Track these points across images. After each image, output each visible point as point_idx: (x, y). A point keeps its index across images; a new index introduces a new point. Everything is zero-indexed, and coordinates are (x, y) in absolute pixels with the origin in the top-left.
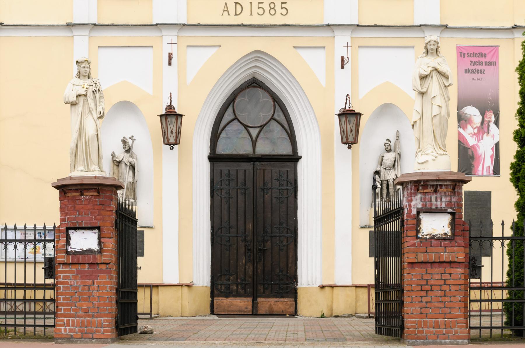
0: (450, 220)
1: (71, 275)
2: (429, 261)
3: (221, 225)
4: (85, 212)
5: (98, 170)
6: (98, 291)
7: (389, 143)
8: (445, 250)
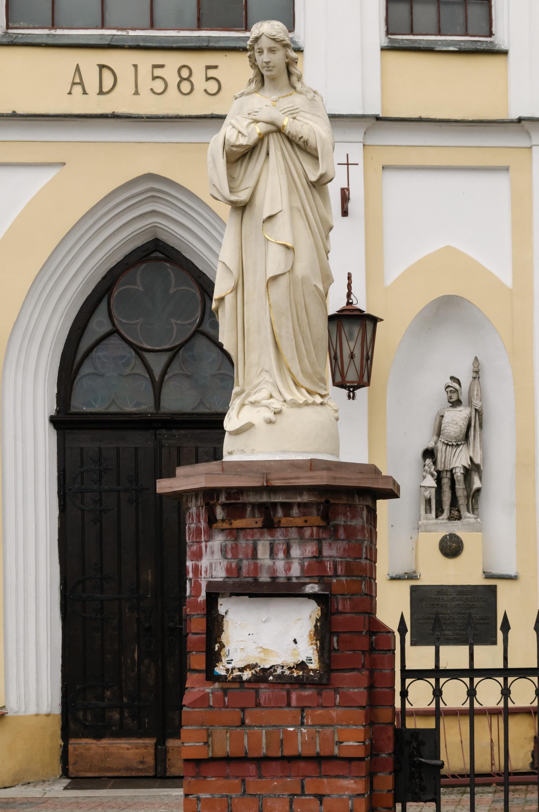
0: (317, 620)
2: (250, 755)
7: (456, 385)
8: (303, 718)
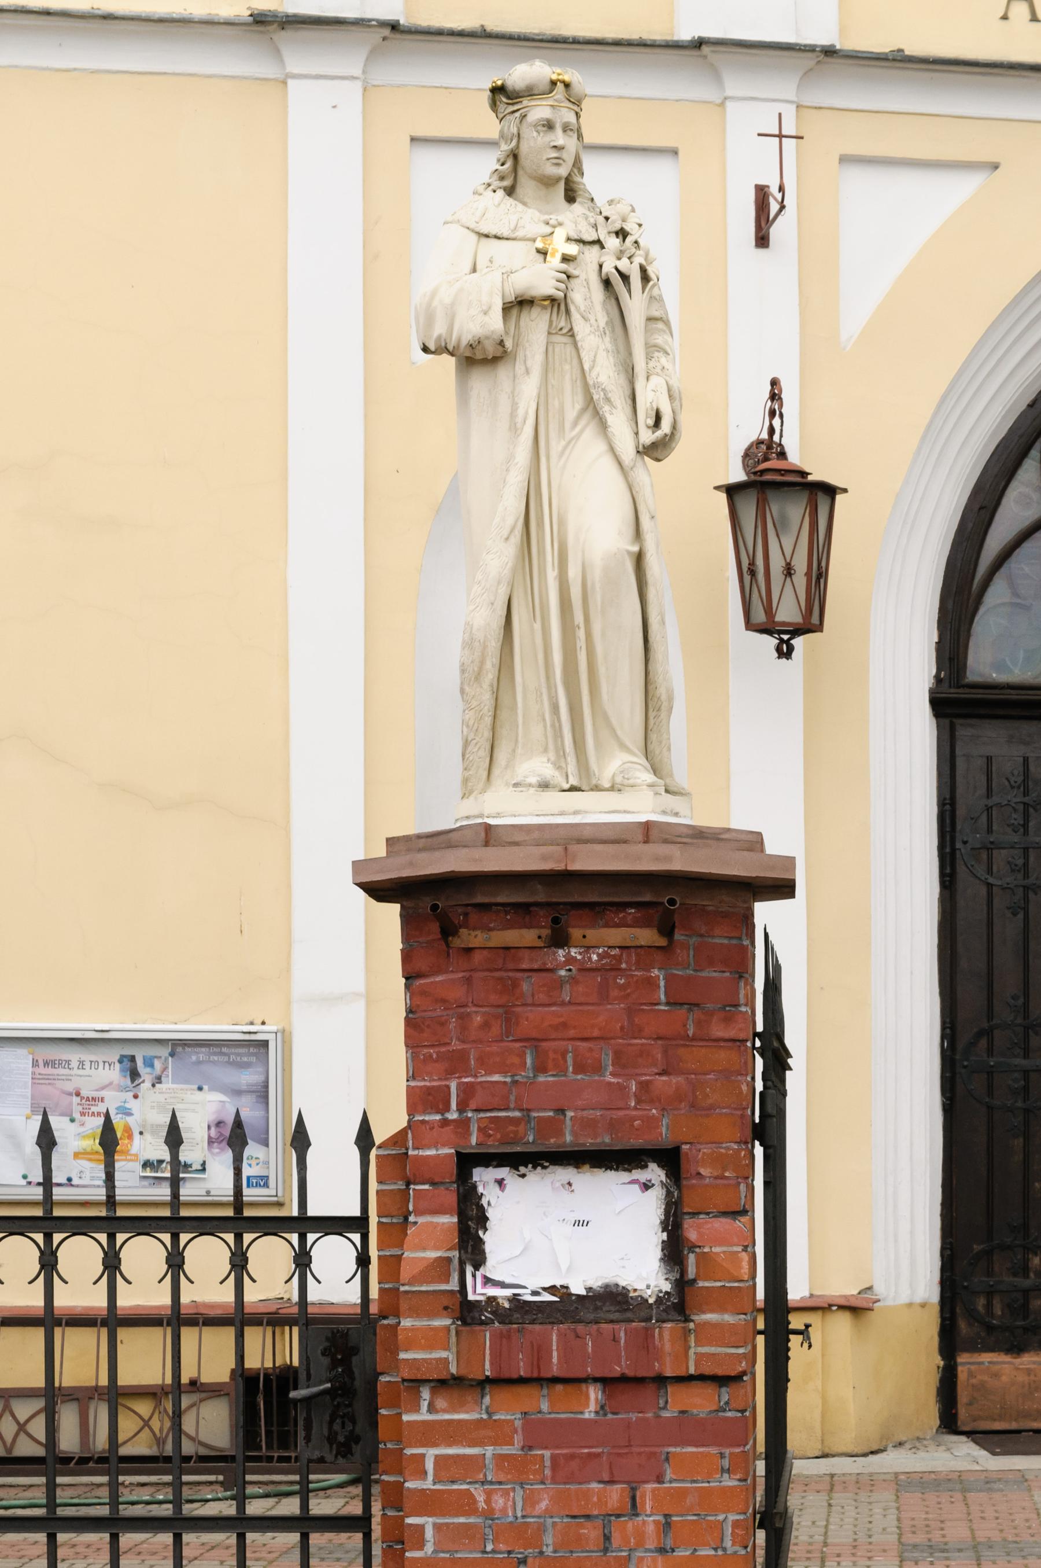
1: (489, 1451)
3: (990, 1016)
4: (575, 1051)
5: (651, 785)
6: (662, 1550)
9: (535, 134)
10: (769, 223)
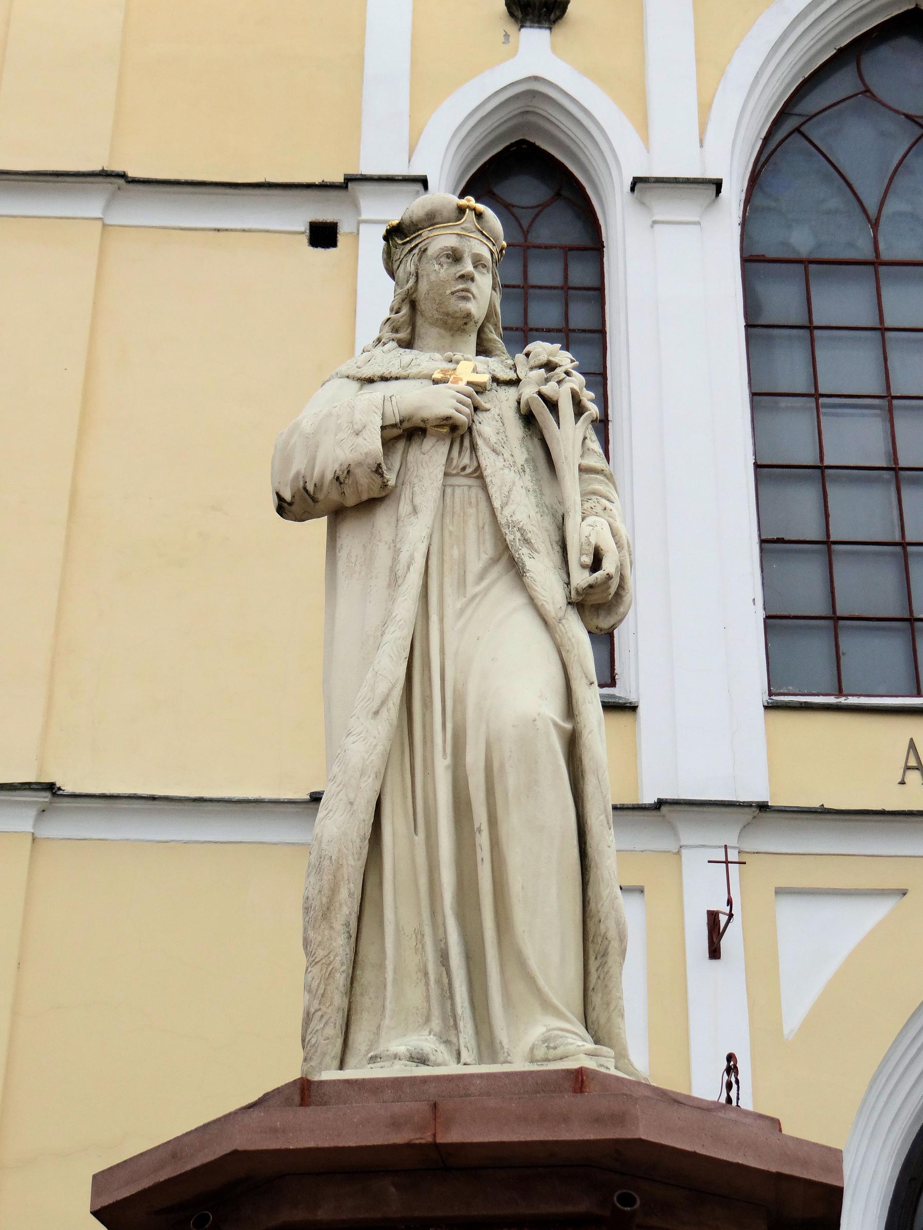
9: (437, 267)
10: (720, 935)
